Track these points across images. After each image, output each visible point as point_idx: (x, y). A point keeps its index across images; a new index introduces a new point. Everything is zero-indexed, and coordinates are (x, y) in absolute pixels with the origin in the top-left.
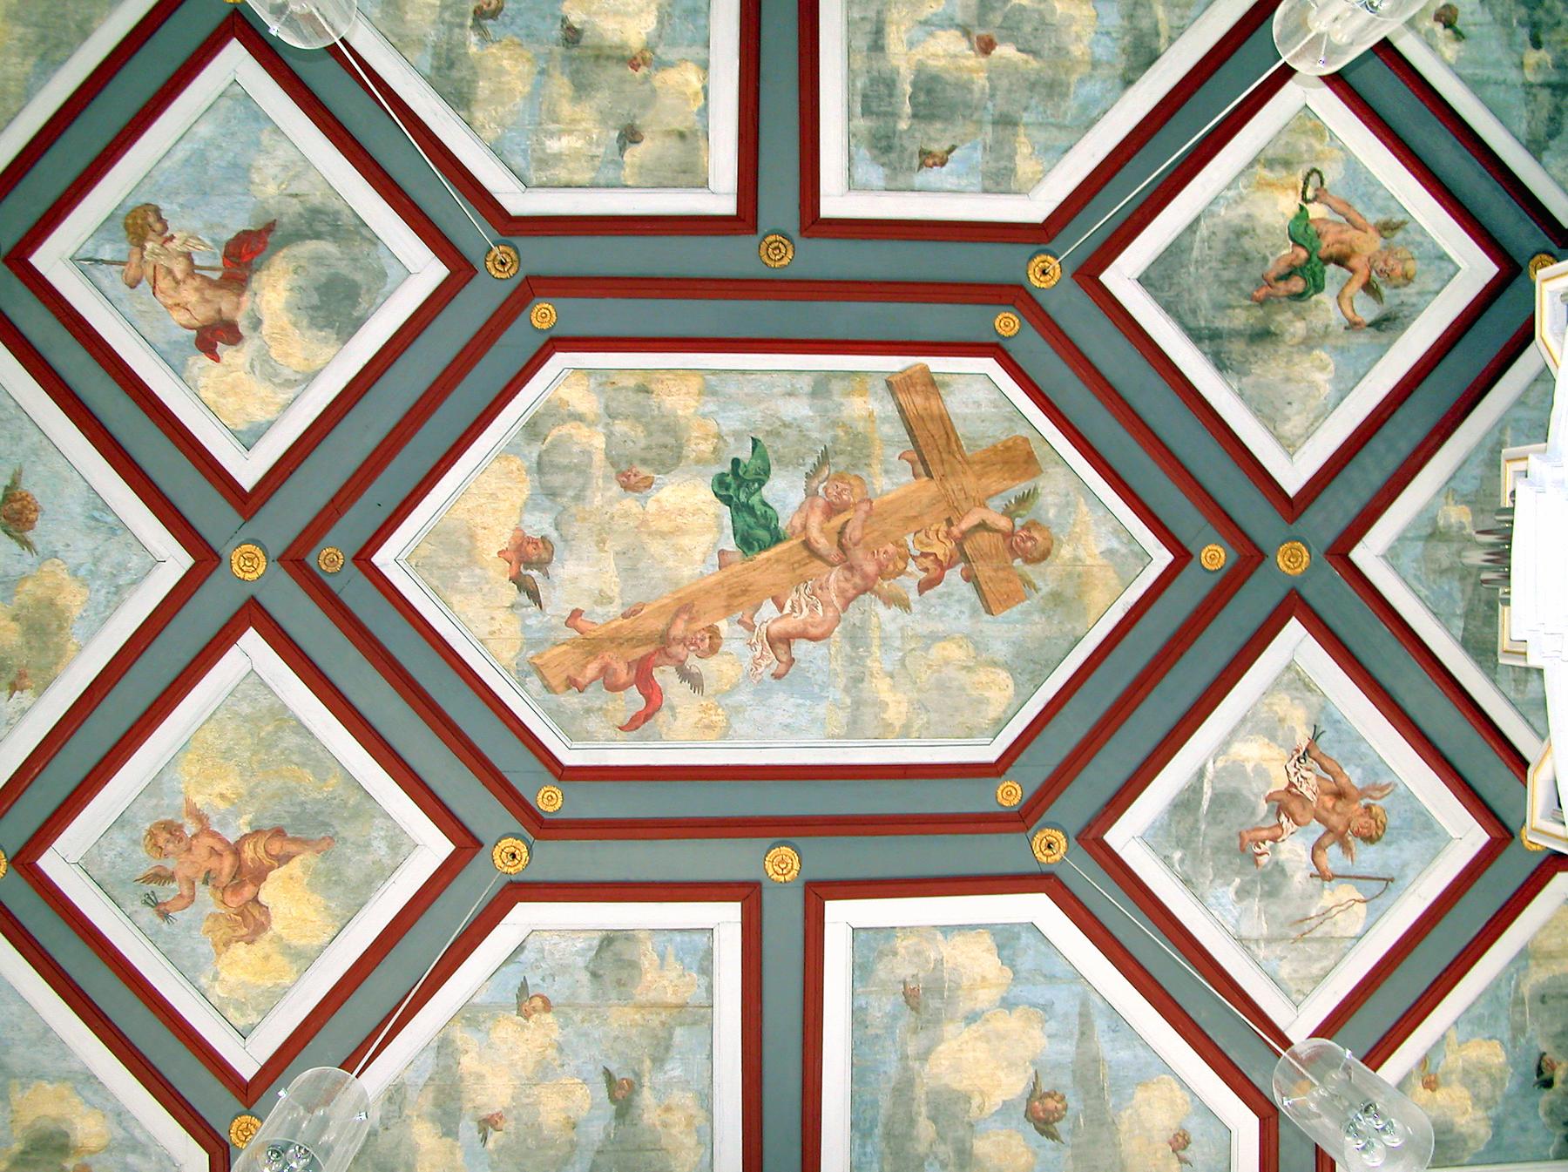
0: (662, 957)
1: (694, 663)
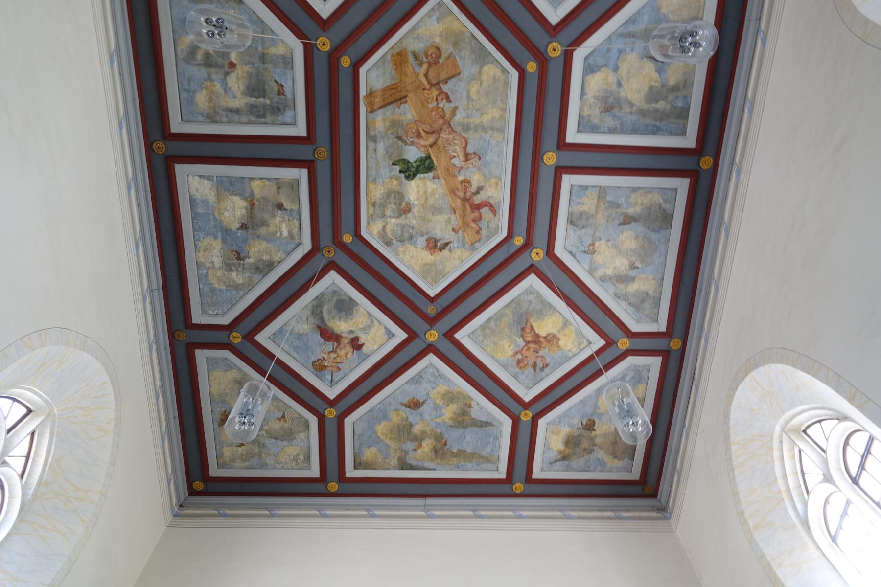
0: (580, 203)
1: (474, 189)
